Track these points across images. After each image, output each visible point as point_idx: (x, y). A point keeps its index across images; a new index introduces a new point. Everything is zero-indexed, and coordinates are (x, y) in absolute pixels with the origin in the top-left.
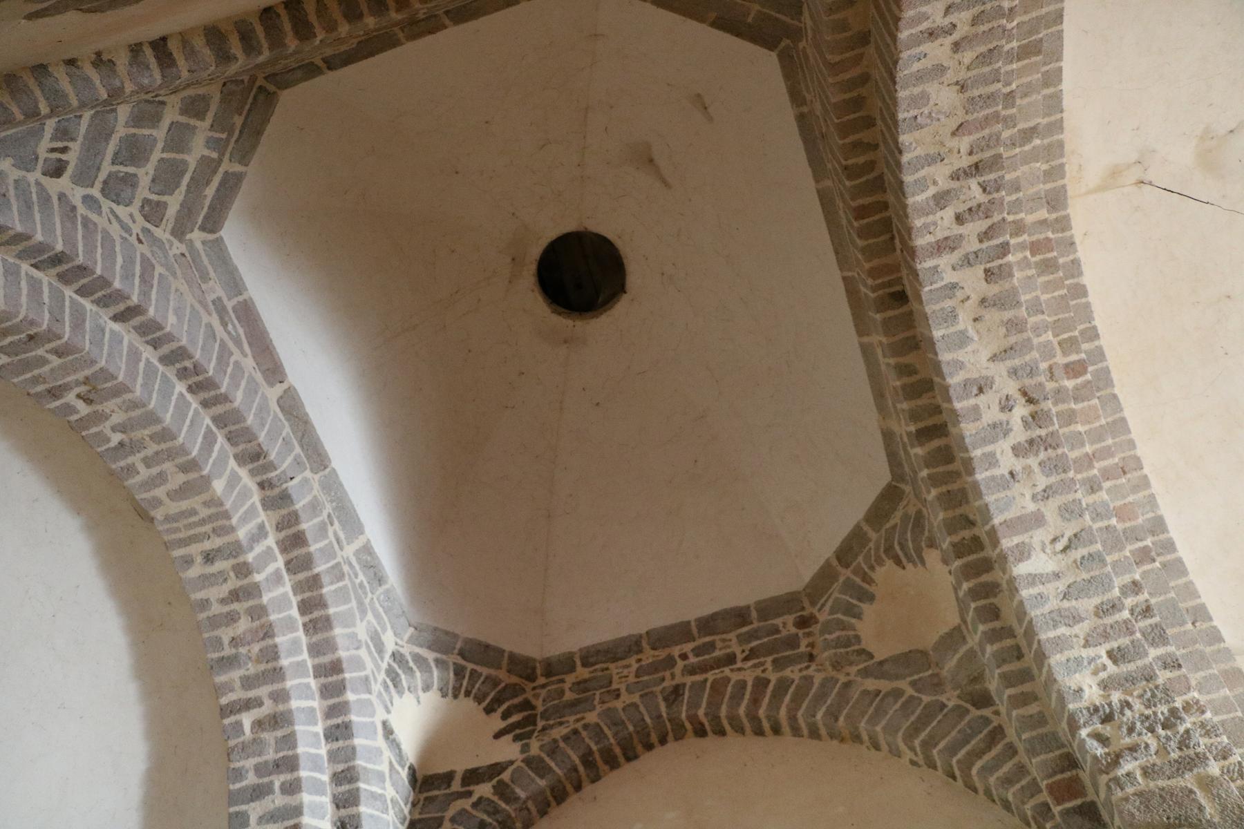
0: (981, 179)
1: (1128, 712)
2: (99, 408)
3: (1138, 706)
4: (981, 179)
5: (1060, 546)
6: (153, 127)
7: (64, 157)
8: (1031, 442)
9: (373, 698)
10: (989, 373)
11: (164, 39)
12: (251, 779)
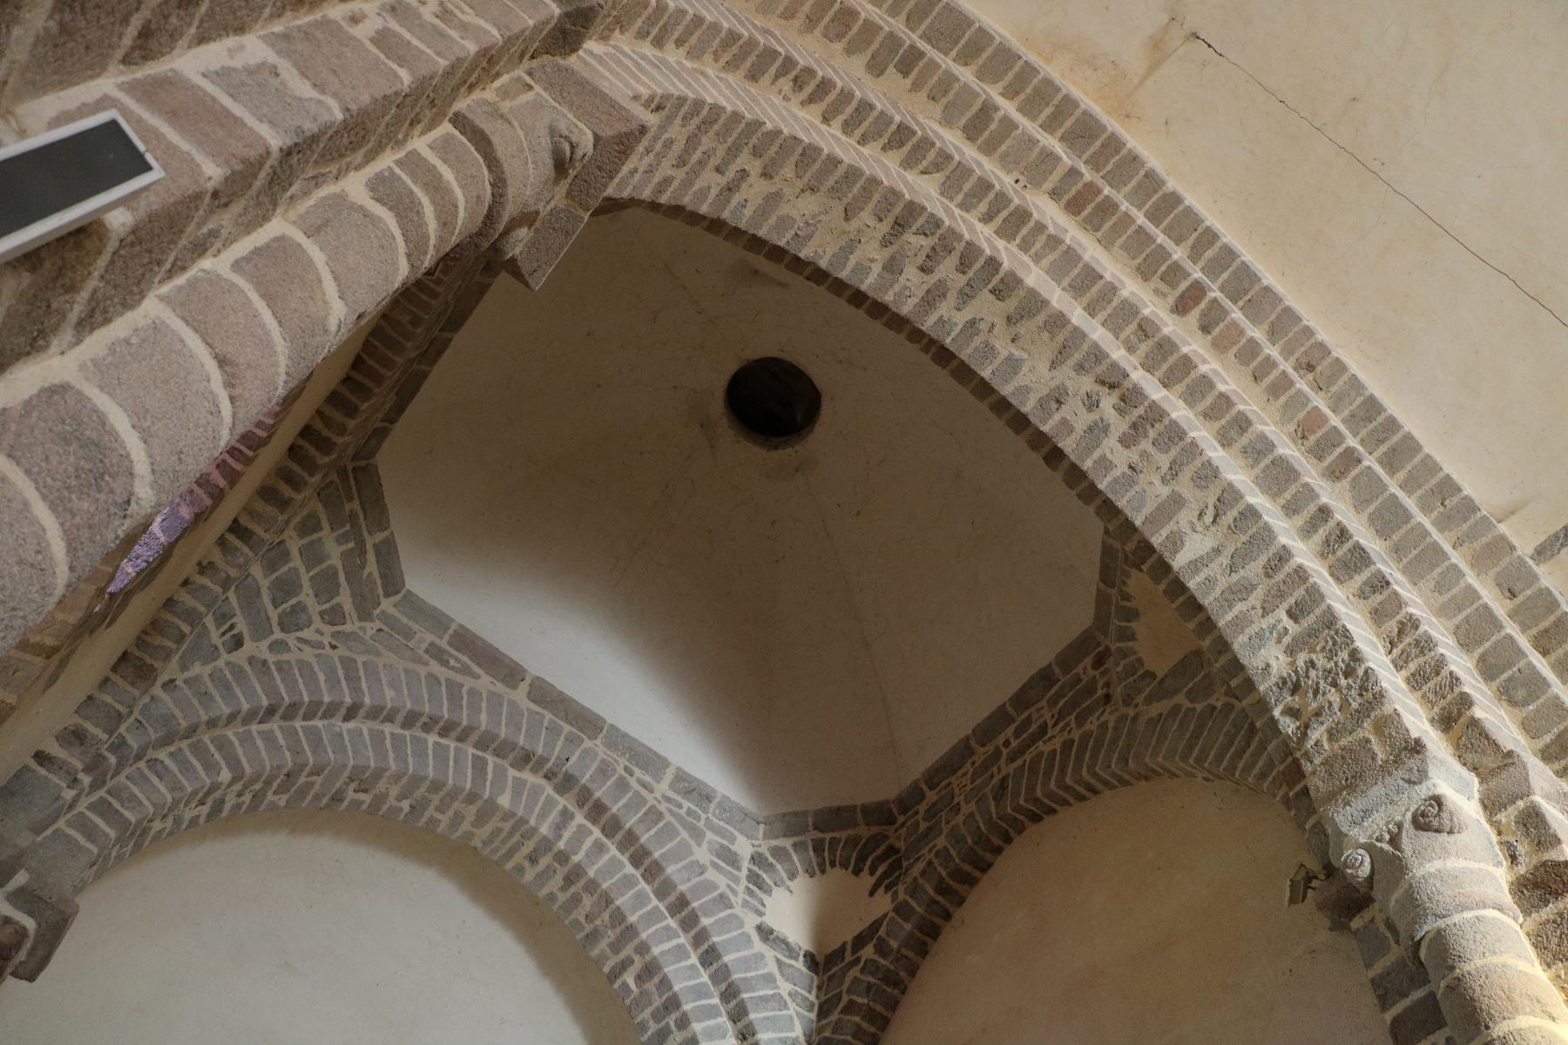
0: (914, 229)
1: (1313, 673)
2: (376, 791)
3: (1321, 661)
4: (914, 229)
5: (1208, 519)
6: (287, 562)
7: (235, 632)
8: (1134, 426)
9: (738, 910)
10: (1057, 382)
11: (235, 521)
12: (653, 1027)
